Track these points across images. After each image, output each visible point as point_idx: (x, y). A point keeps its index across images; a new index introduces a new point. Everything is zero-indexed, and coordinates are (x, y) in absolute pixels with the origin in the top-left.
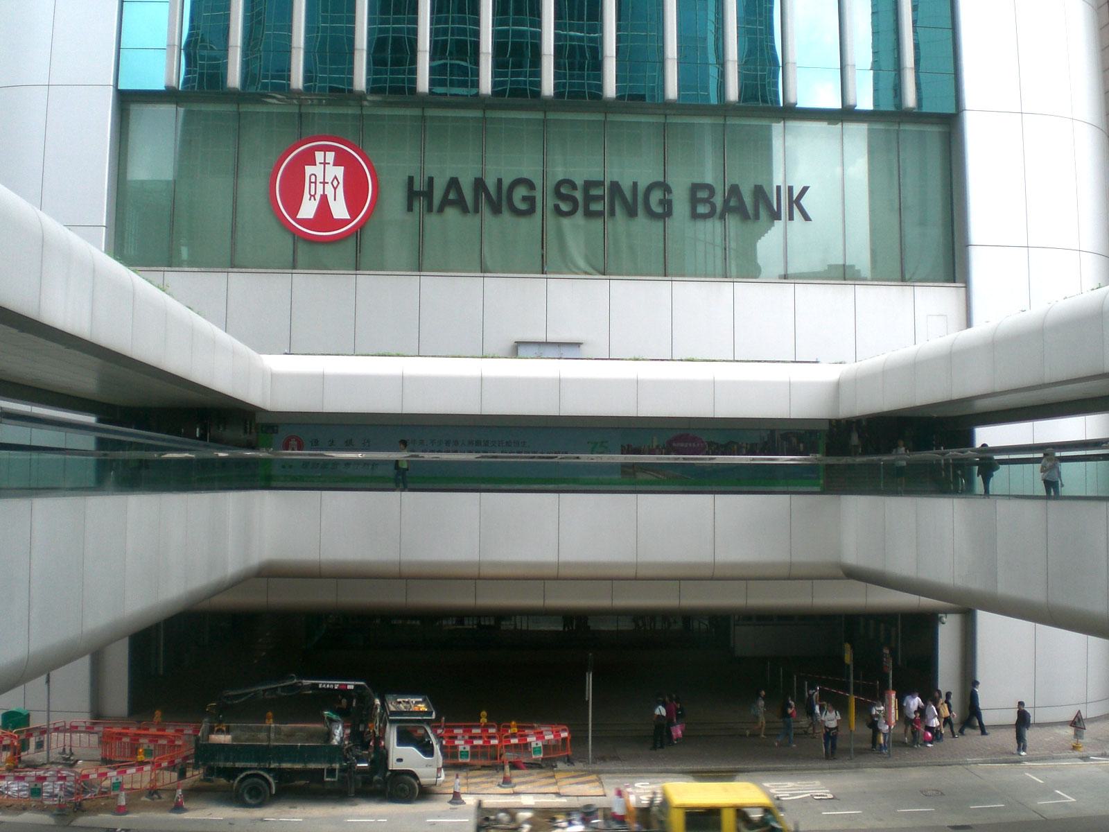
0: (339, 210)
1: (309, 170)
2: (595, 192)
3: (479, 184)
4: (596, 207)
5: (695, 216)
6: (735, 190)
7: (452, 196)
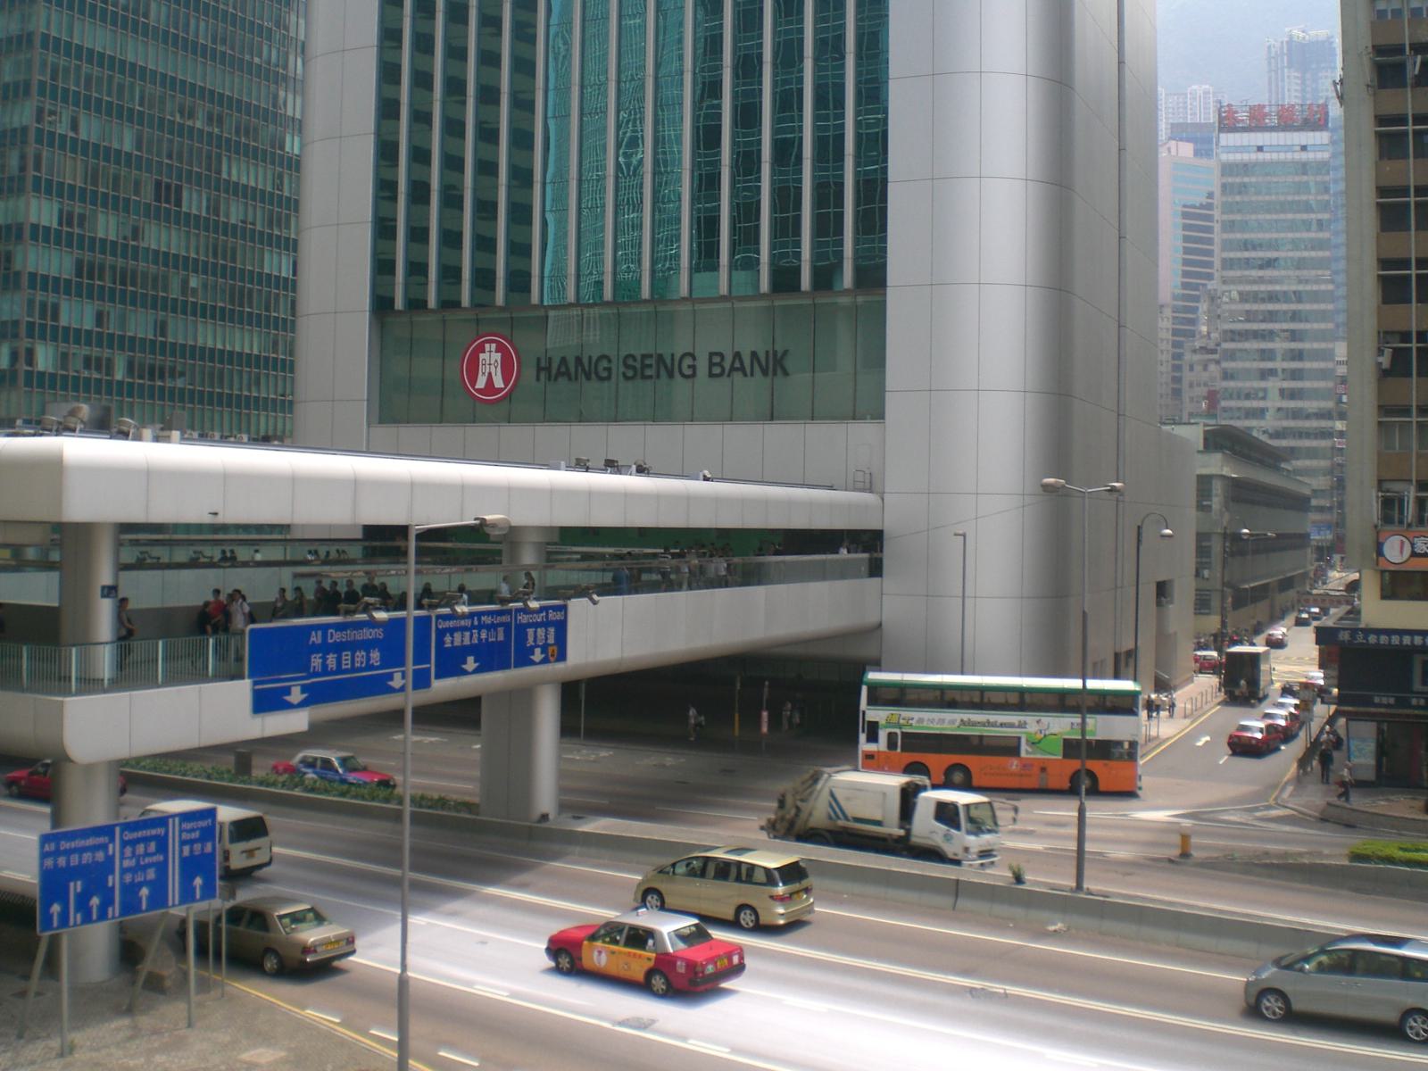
0: (498, 382)
1: (482, 356)
2: (648, 362)
3: (579, 360)
4: (648, 372)
5: (711, 375)
6: (737, 355)
7: (563, 369)
